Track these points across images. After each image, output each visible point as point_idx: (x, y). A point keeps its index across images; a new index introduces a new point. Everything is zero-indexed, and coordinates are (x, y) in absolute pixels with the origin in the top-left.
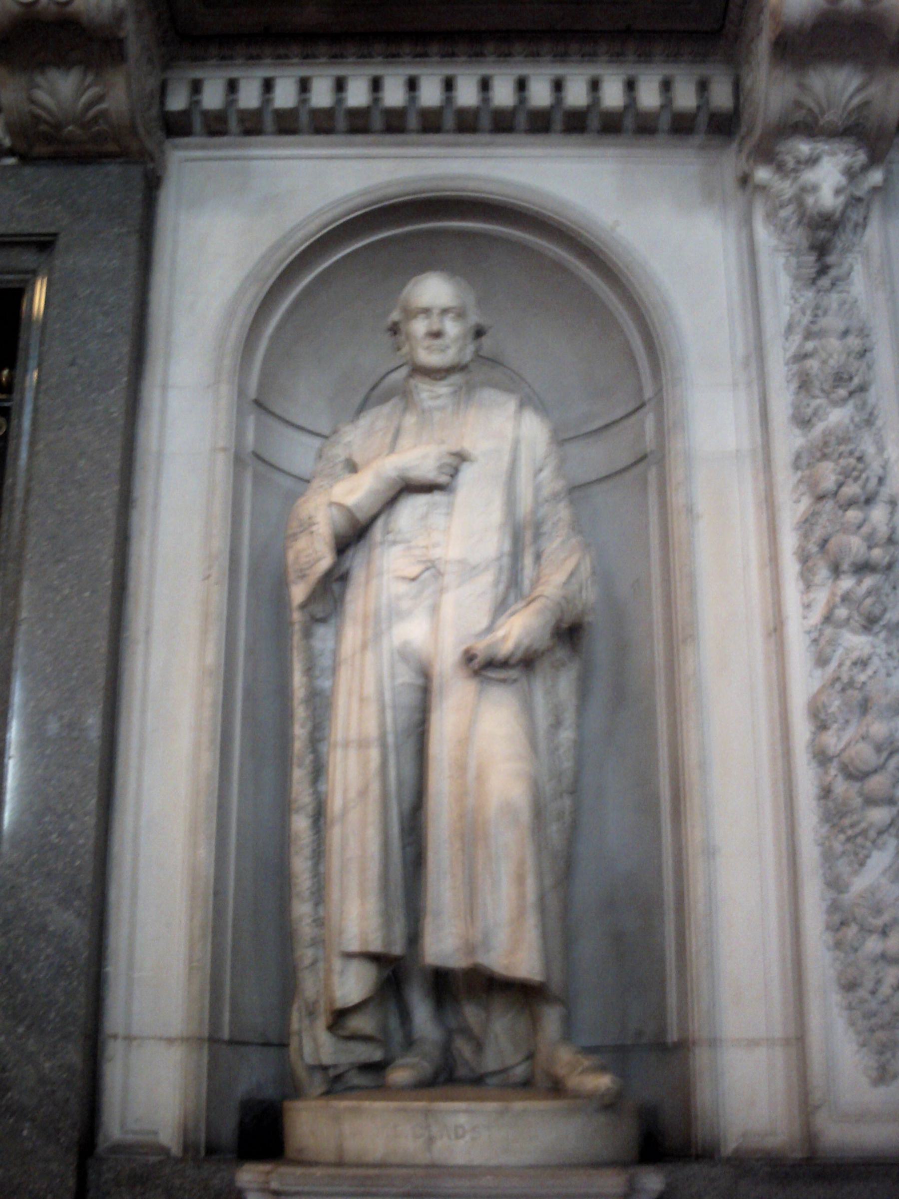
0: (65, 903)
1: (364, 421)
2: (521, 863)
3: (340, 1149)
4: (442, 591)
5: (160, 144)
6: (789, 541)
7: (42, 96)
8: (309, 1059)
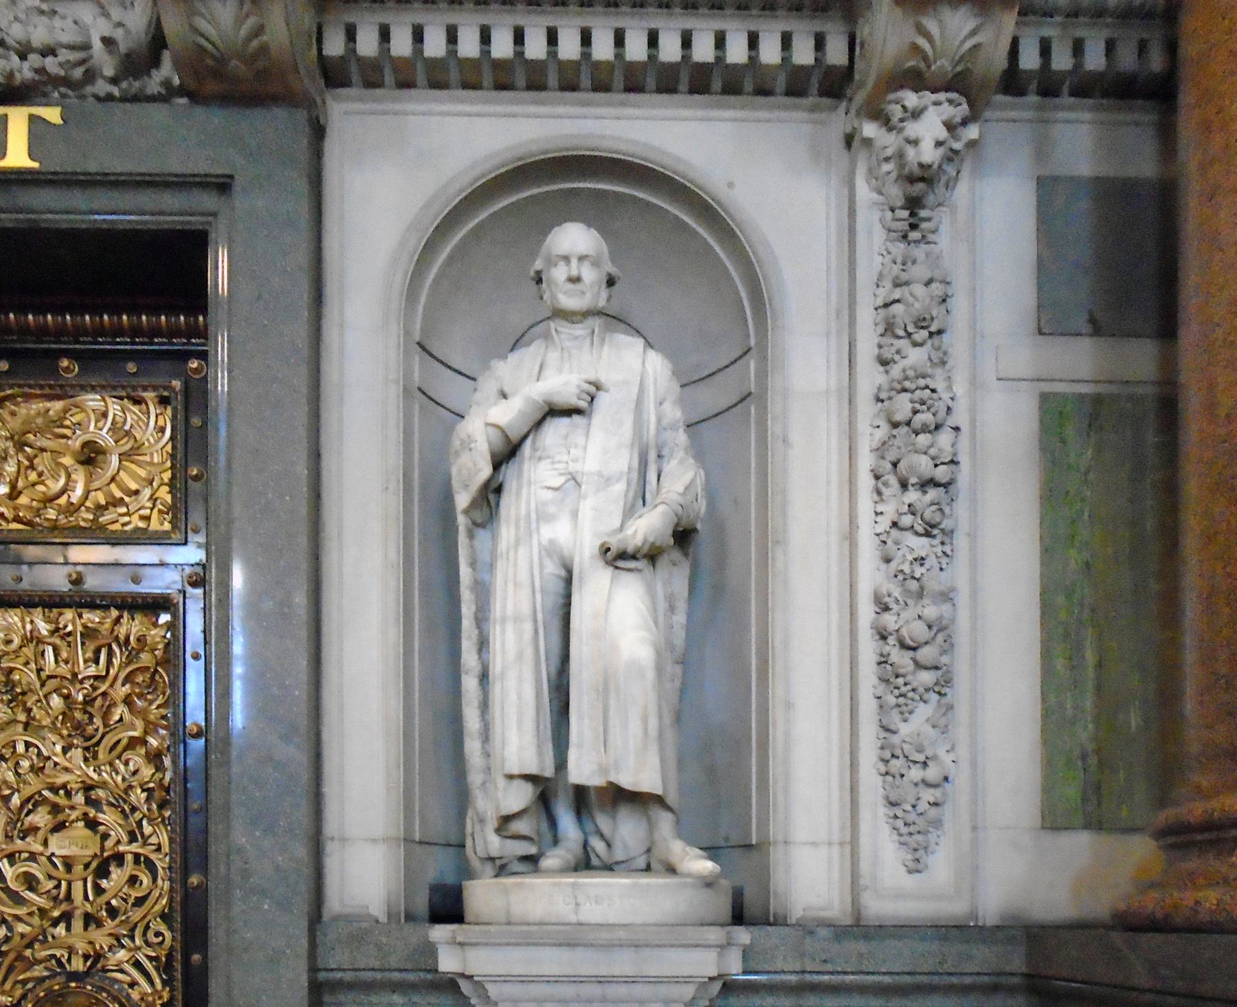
0: (286, 738)
1: (513, 358)
3: (508, 912)
4: (581, 497)
5: (321, 94)
6: (866, 461)
7: (202, 24)
8: (482, 854)
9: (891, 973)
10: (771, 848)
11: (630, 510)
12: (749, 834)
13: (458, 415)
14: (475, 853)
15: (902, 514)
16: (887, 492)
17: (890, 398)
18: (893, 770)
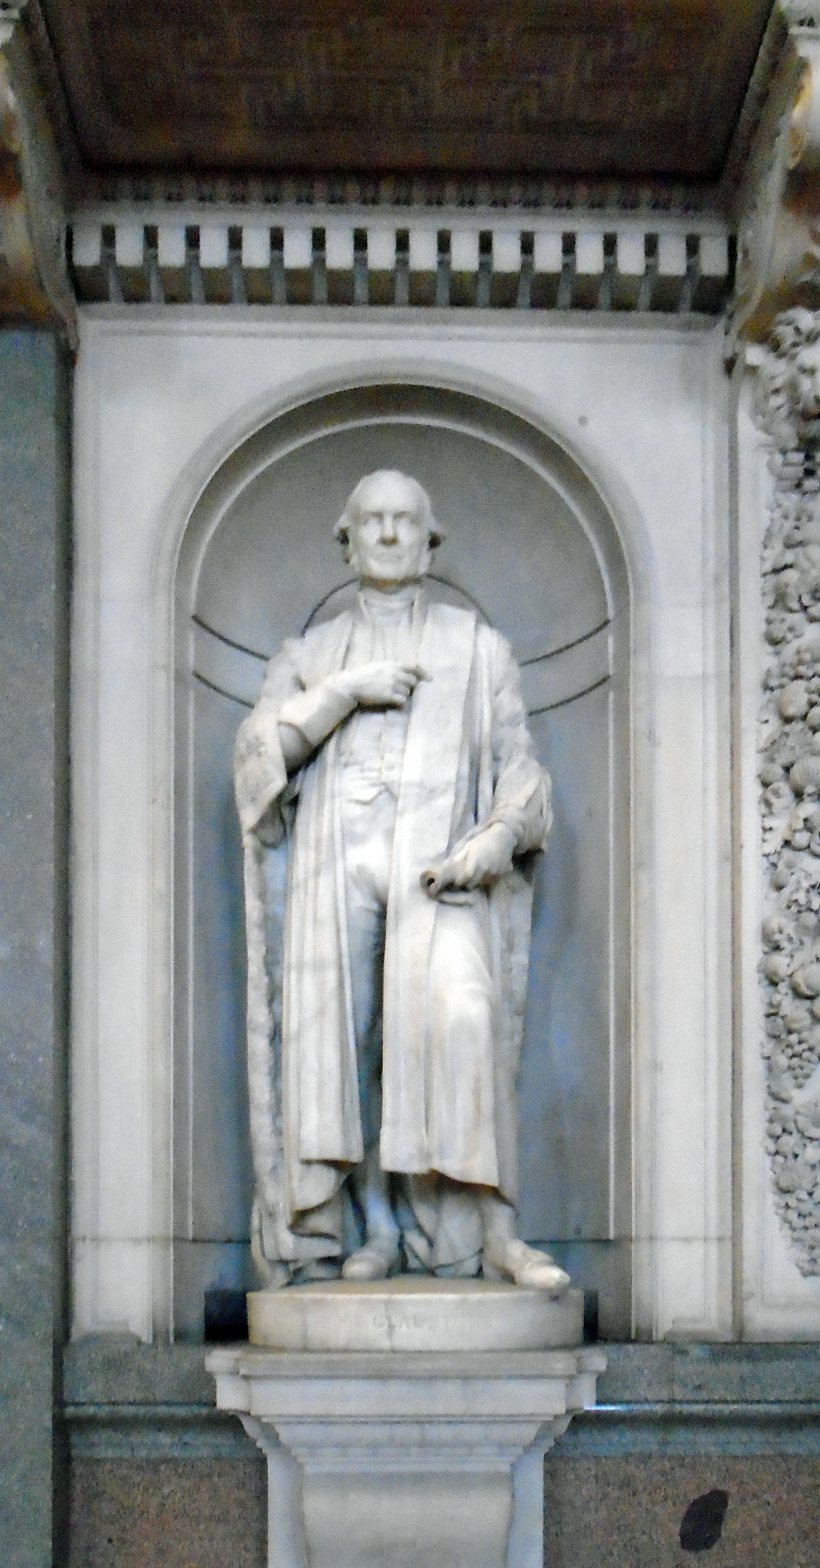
0: (26, 1118)
1: (312, 635)
2: (477, 1080)
3: (305, 1336)
4: (396, 813)
9: (778, 1402)
10: (633, 1247)
11: (457, 830)
12: (607, 1229)
13: (242, 702)
14: (263, 1254)
15: (795, 831)
16: (777, 803)
17: (782, 686)
18: (785, 1149)
